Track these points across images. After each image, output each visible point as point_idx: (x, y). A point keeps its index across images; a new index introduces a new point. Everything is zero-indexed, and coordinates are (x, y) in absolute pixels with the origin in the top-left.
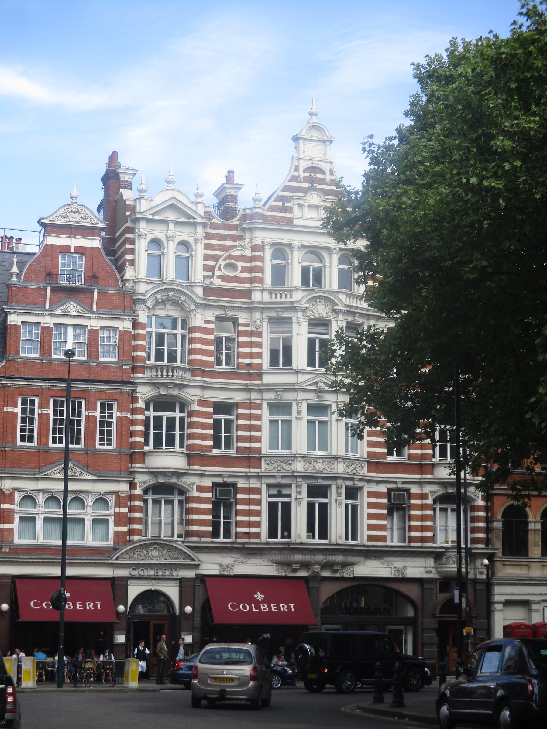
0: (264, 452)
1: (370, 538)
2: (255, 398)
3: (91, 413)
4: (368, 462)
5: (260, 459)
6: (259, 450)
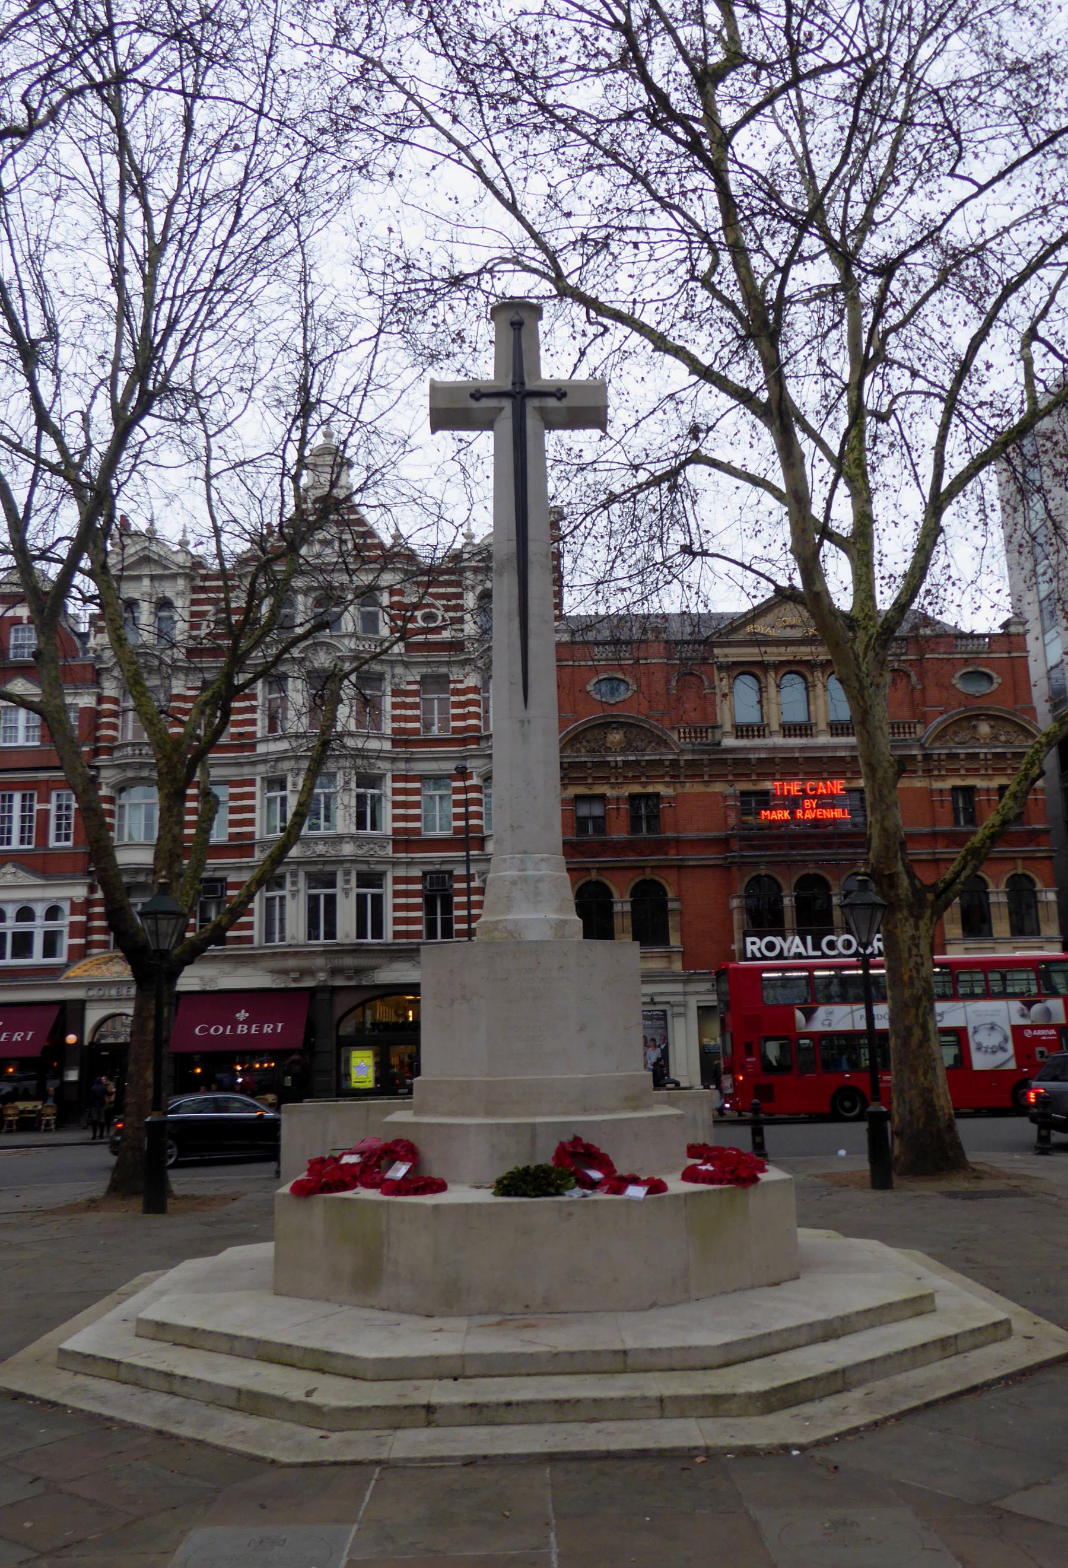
0: (257, 836)
1: (397, 934)
2: (246, 772)
3: (43, 806)
4: (394, 841)
5: (252, 846)
6: (251, 835)
